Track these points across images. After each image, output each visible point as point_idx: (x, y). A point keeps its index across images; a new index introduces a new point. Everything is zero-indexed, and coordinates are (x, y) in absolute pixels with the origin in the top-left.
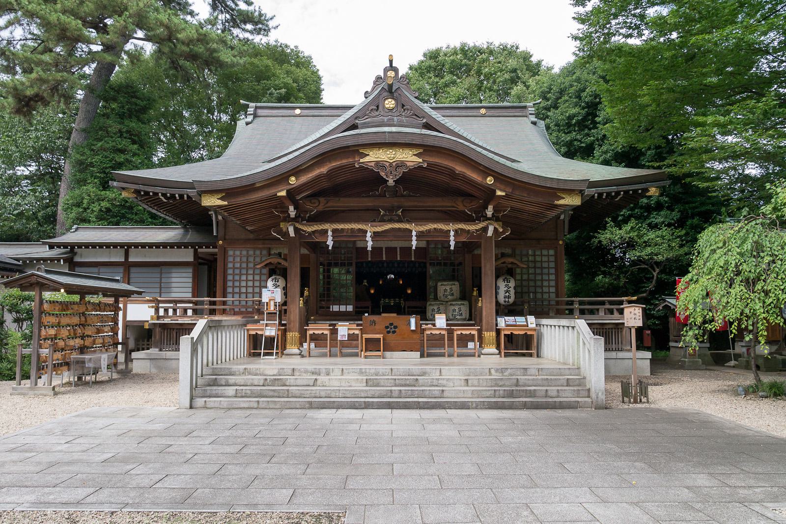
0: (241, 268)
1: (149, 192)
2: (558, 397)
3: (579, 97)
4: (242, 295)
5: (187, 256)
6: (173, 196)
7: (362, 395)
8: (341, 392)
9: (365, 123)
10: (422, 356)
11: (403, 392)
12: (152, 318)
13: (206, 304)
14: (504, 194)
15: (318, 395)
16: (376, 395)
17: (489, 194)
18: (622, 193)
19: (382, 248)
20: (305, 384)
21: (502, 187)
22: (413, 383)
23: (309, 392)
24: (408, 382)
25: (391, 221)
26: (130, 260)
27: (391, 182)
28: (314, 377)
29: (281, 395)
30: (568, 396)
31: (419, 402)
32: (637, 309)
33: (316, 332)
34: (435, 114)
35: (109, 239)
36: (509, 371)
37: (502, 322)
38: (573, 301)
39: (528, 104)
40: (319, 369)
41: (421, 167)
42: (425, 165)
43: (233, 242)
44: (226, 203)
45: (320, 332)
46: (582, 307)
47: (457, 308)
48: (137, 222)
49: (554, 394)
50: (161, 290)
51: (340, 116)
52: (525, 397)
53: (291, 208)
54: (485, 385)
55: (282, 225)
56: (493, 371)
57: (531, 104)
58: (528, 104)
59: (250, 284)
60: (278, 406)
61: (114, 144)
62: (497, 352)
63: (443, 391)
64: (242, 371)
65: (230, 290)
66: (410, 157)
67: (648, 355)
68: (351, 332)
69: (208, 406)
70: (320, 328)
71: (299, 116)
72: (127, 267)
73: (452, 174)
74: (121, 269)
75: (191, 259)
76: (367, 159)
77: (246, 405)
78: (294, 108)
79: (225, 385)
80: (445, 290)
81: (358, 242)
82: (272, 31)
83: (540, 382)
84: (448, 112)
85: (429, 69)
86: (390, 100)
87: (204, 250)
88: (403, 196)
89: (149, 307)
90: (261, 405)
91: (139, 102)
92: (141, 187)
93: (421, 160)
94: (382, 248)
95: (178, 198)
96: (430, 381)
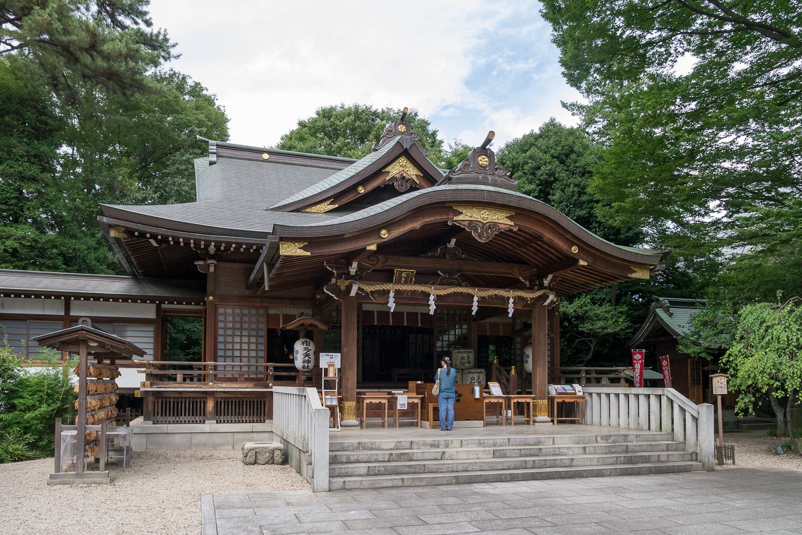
0: (234, 329)
2: (668, 461)
3: (534, 174)
5: (149, 312)
7: (499, 468)
8: (478, 465)
9: (459, 178)
10: (217, 423)
11: (537, 462)
15: (455, 469)
16: (512, 466)
19: (373, 312)
20: (433, 458)
21: (585, 257)
22: (537, 453)
23: (446, 466)
24: (532, 452)
25: (451, 284)
29: (417, 471)
30: (676, 461)
31: (560, 472)
32: (723, 378)
33: (374, 401)
36: (613, 438)
37: (554, 389)
38: (581, 370)
40: (438, 441)
41: (511, 231)
42: (515, 230)
43: (224, 299)
44: (309, 254)
45: (377, 401)
46: (588, 376)
47: (475, 376)
48: (49, 268)
49: (665, 459)
51: (341, 170)
52: (642, 463)
54: (600, 452)
56: (599, 439)
59: (245, 346)
60: (423, 484)
61: (21, 169)
62: (550, 419)
63: (572, 459)
64: (355, 445)
65: (220, 353)
66: (502, 219)
68: (411, 401)
69: (347, 487)
70: (375, 397)
75: (152, 315)
76: (460, 218)
77: (389, 484)
79: (347, 463)
80: (463, 358)
81: (364, 305)
82: (173, 59)
83: (645, 448)
85: (323, 129)
86: (484, 157)
88: (461, 259)
89: (138, 372)
90: (406, 483)
91: (50, 121)
93: (512, 224)
94: (373, 312)
96: (552, 450)
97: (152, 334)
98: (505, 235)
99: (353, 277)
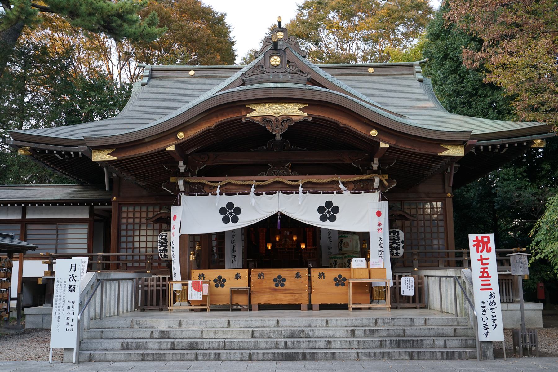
1: (44, 150)
4: (129, 250)
6: (68, 153)
9: (251, 80)
12: (46, 273)
13: (99, 260)
14: (388, 146)
17: (374, 143)
18: (507, 145)
21: (387, 139)
26: (27, 217)
27: (278, 137)
28: (151, 330)
34: (322, 72)
35: (7, 197)
38: (462, 253)
39: (415, 63)
42: (310, 119)
44: (116, 158)
50: (57, 247)
53: (181, 163)
55: (172, 180)
56: (379, 323)
57: (418, 63)
58: (415, 63)
65: (123, 245)
66: (294, 111)
67: (541, 306)
71: (193, 77)
72: (24, 223)
73: (335, 126)
74: (18, 226)
75: (87, 216)
78: (190, 69)
84: (337, 72)
86: (275, 57)
87: (99, 207)
92: (36, 145)
93: (306, 115)
95: (73, 156)
97: (86, 231)
98: (304, 122)
99: (375, 172)
